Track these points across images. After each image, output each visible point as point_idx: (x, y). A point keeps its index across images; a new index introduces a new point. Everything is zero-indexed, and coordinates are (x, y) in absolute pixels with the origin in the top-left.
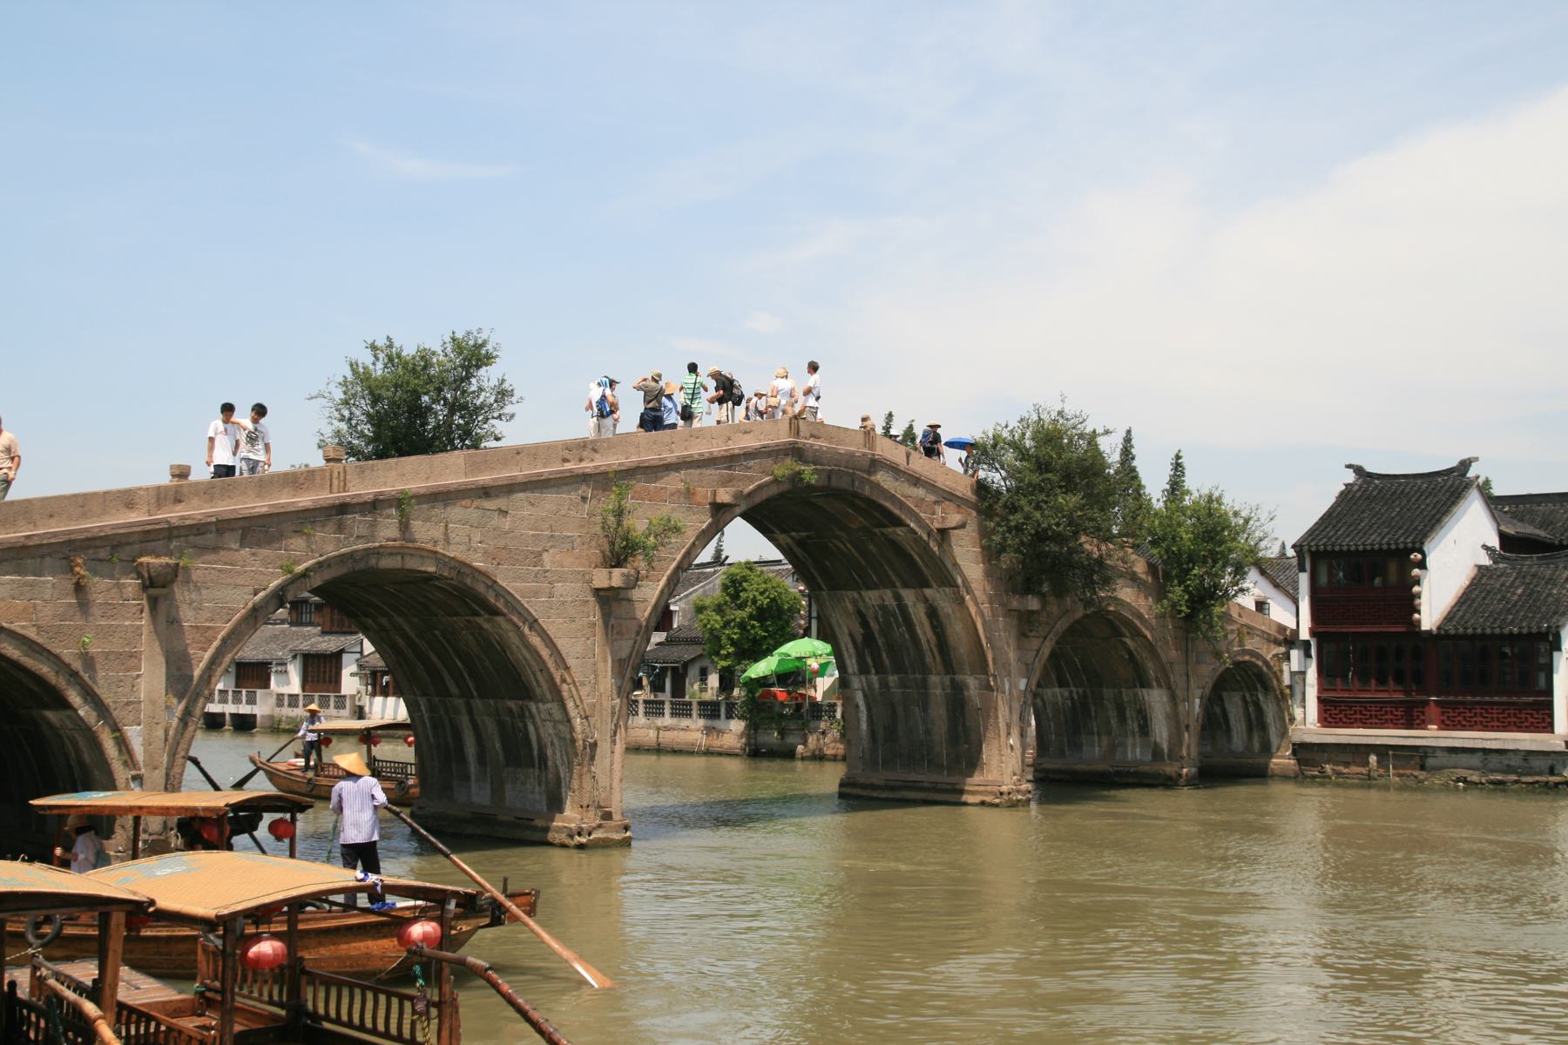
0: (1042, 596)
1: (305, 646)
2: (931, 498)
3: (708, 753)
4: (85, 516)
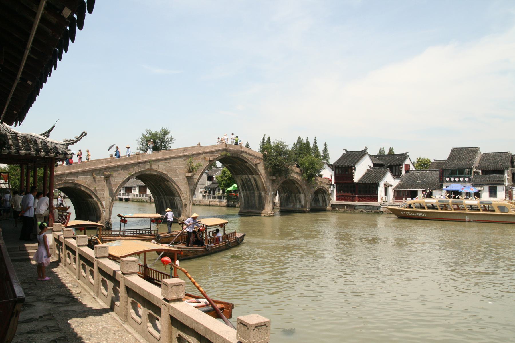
0: (276, 176)
1: (139, 184)
2: (254, 158)
3: (219, 206)
4: (95, 165)
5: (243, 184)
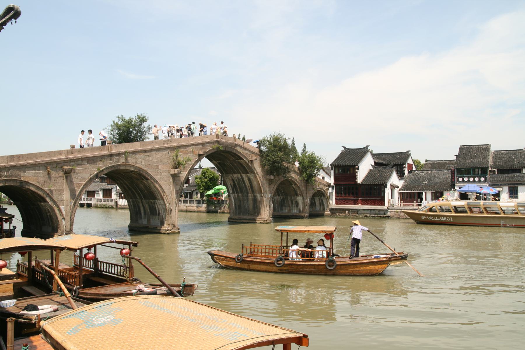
0: (274, 176)
1: (103, 188)
2: (249, 153)
3: (198, 212)
4: (50, 157)
5: (235, 185)
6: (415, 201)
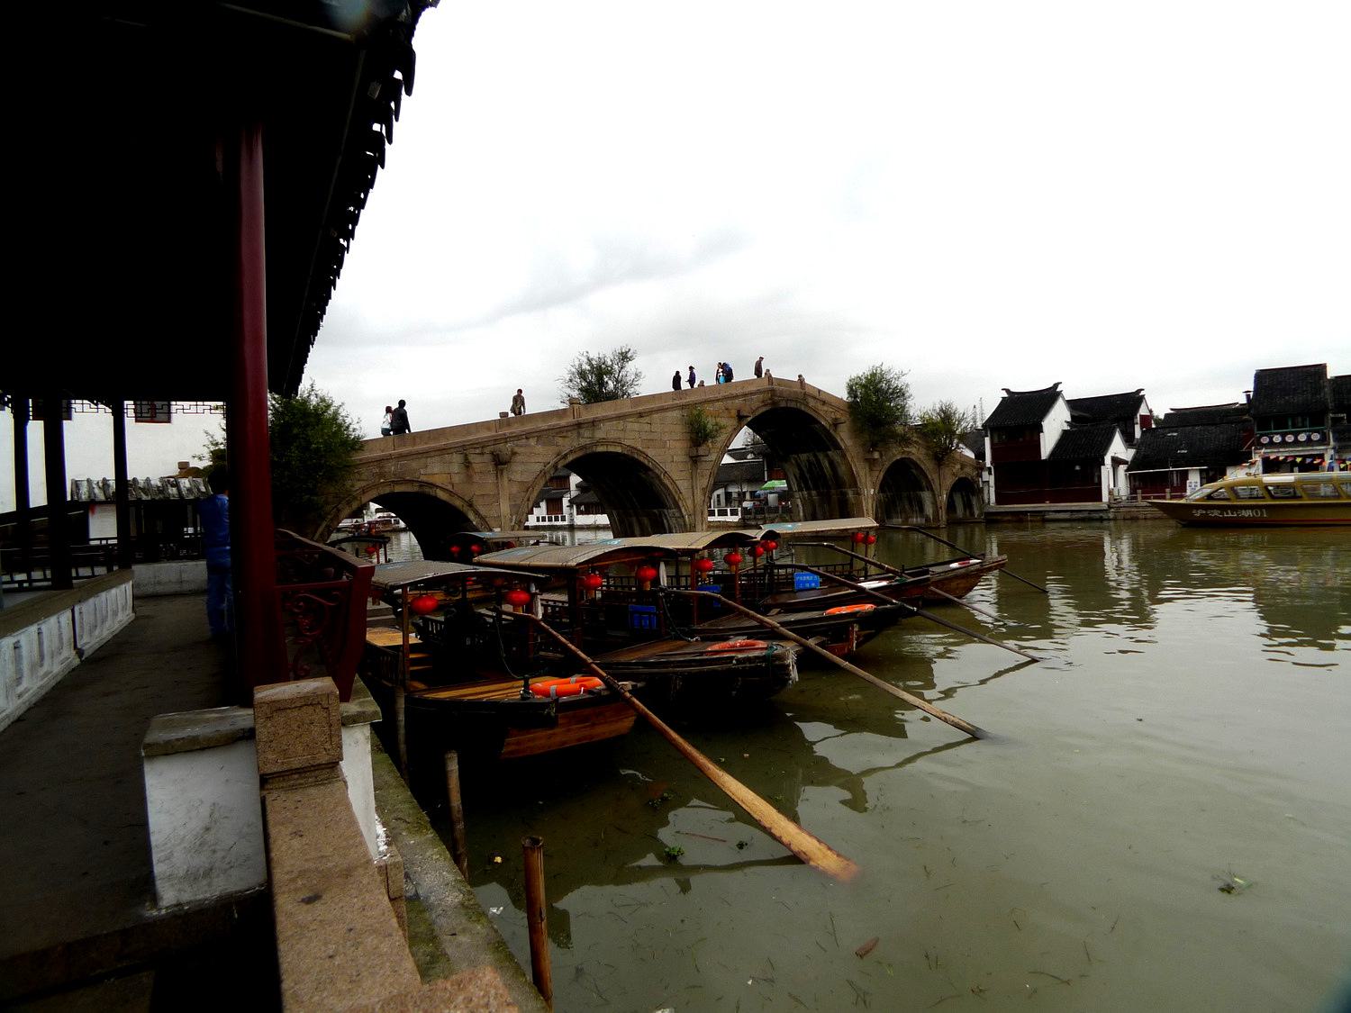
6: (1168, 490)
